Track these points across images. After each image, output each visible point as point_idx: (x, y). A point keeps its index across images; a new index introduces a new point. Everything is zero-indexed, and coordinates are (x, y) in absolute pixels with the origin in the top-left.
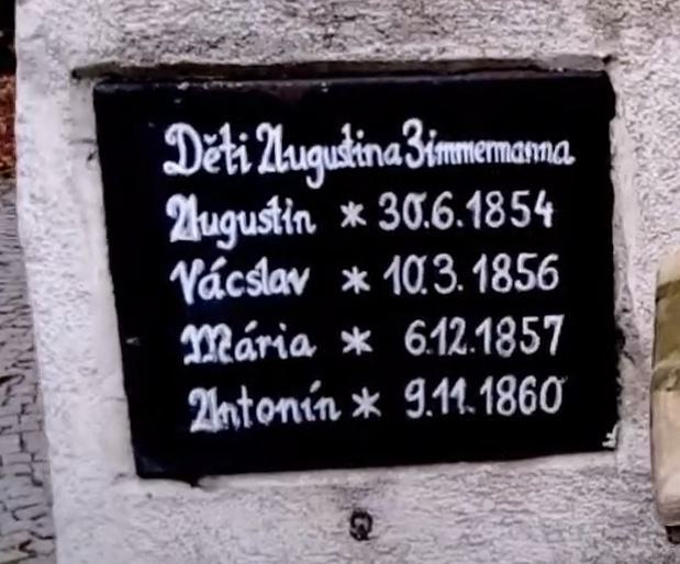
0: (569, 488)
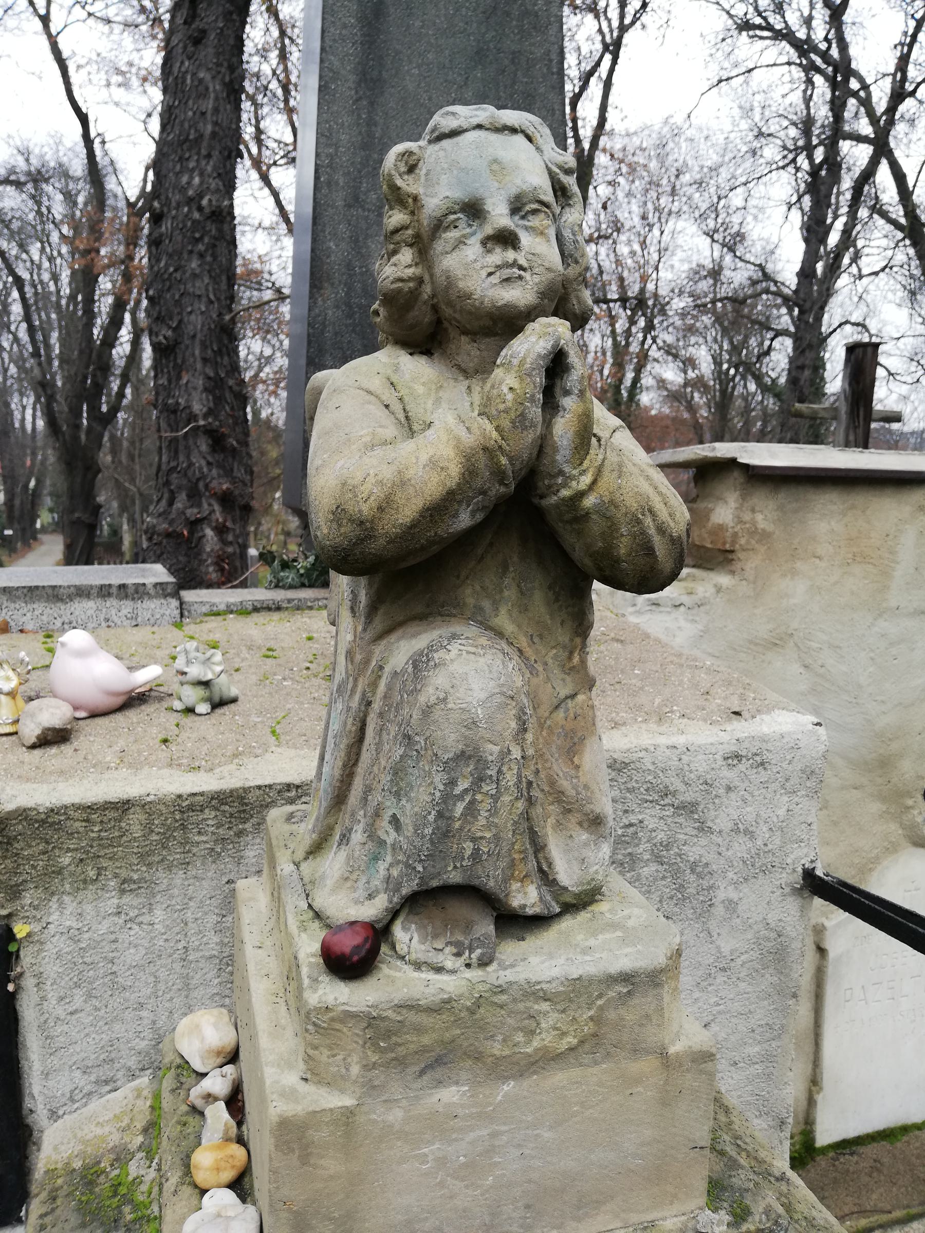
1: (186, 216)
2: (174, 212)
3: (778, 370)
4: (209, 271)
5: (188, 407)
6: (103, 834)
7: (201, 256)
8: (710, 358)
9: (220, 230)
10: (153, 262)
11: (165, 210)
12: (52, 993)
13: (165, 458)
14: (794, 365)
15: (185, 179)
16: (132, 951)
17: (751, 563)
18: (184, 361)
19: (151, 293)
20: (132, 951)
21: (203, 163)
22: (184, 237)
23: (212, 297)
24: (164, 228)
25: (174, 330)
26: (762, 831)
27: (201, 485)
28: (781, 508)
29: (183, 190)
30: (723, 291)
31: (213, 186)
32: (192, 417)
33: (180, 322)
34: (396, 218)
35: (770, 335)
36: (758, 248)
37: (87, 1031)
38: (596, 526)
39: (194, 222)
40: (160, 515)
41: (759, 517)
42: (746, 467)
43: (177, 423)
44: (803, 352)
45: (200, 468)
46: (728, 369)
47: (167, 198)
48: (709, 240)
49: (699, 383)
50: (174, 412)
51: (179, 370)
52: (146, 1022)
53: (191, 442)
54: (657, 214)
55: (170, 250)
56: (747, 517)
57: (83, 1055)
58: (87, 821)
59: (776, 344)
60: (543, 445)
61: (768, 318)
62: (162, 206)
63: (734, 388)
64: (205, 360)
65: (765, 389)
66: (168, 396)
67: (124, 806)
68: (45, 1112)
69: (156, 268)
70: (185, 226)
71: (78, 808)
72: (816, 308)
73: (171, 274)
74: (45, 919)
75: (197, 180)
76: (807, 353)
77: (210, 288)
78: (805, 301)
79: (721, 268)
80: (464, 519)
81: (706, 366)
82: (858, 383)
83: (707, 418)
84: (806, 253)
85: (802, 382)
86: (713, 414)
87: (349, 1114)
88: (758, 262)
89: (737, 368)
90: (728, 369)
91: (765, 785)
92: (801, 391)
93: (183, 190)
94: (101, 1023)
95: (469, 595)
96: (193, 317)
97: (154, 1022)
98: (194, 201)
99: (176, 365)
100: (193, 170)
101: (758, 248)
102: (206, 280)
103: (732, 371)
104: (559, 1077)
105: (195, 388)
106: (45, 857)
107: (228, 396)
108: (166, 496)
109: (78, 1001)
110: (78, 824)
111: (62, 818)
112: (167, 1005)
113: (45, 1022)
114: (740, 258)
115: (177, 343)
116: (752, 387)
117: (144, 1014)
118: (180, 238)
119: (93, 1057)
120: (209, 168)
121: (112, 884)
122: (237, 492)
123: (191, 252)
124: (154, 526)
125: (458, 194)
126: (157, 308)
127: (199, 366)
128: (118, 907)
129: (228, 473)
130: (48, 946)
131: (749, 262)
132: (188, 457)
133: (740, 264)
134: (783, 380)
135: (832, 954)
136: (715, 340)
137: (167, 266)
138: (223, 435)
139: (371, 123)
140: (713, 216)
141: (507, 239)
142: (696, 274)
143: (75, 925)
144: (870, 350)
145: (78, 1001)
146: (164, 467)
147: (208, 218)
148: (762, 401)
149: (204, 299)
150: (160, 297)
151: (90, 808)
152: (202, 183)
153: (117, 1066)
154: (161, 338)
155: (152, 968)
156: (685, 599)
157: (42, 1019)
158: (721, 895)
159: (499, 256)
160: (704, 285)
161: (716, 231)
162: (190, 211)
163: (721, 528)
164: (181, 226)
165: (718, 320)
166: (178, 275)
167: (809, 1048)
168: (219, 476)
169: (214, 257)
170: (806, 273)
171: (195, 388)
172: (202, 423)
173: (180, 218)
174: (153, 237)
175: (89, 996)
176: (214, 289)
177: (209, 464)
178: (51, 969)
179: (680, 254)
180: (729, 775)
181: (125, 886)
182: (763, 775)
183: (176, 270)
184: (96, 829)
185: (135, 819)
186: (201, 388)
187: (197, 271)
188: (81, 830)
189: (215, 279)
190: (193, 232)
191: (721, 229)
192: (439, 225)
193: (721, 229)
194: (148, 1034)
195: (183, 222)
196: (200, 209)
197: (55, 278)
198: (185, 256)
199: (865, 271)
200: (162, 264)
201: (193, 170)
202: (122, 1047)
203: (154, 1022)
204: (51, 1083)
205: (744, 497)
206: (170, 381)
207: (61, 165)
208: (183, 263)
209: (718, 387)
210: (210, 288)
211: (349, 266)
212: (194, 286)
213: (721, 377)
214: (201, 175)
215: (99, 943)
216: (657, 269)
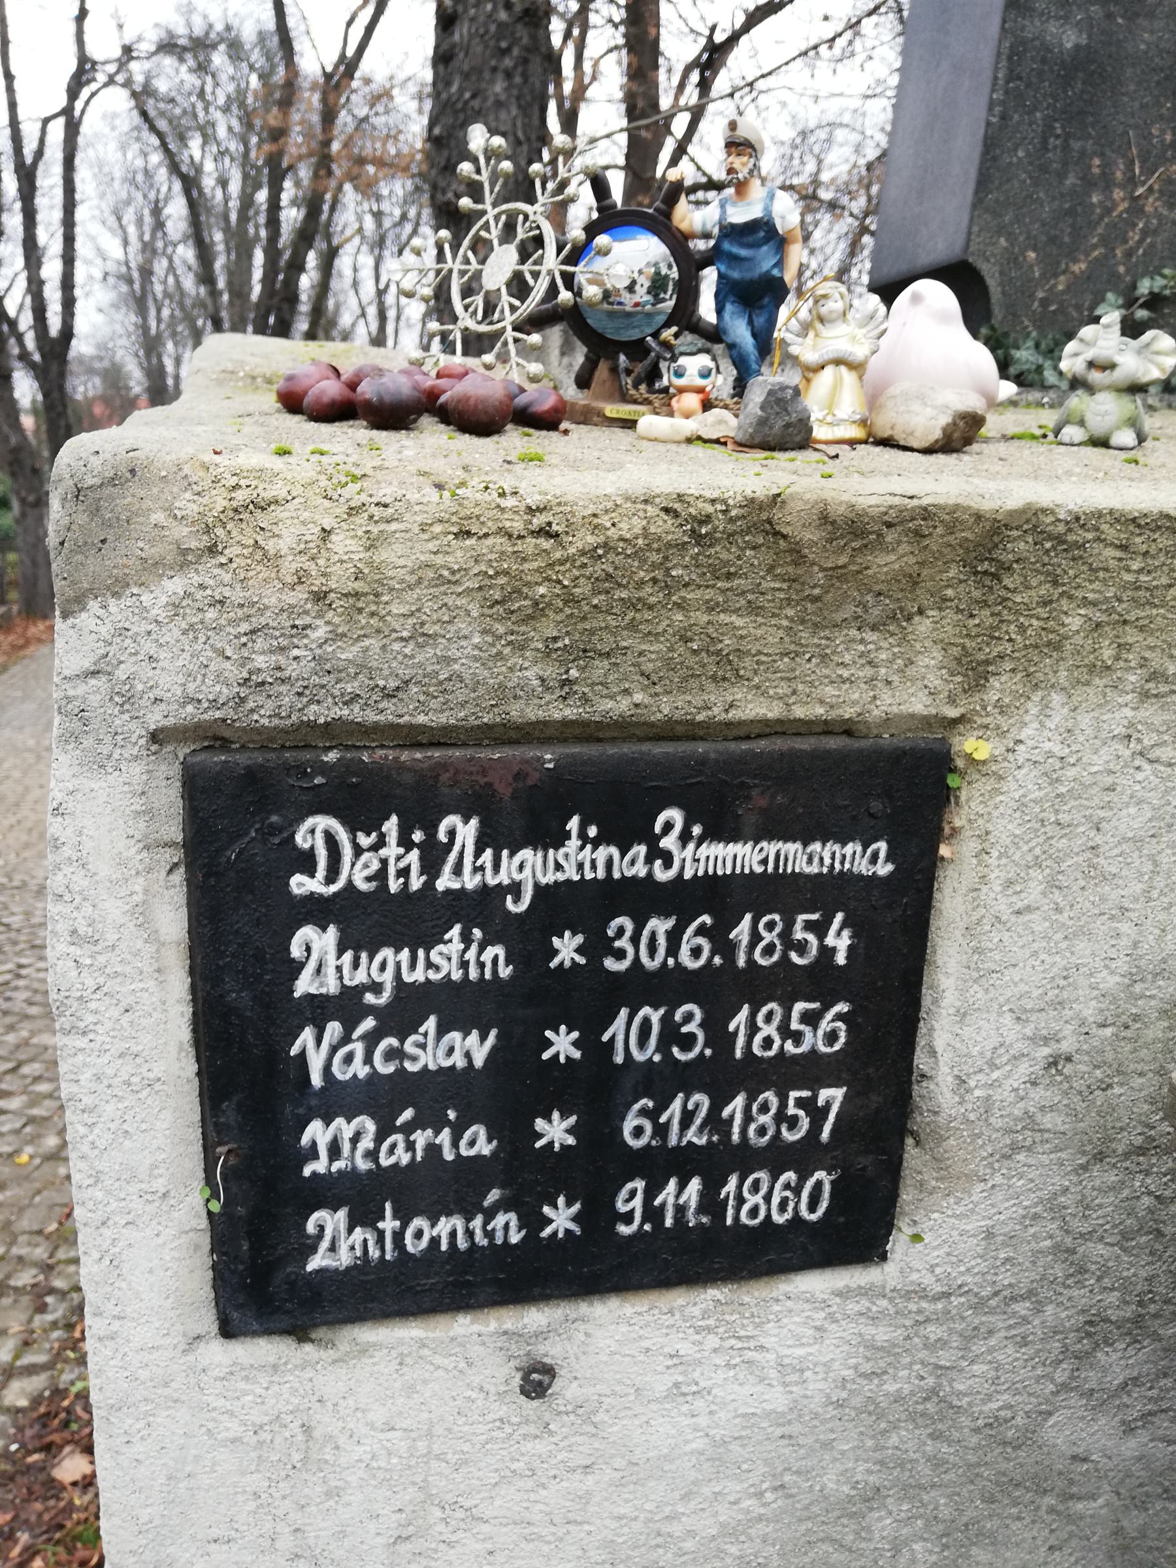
0: (822, 1315)
1: (490, 16)
2: (472, 11)
4: (518, 98)
6: (1144, 578)
7: (508, 75)
10: (440, 86)
11: (460, 8)
12: (997, 872)
16: (1132, 810)
20: (1132, 810)
22: (486, 47)
23: (520, 134)
37: (1036, 946)
39: (501, 25)
52: (1124, 942)
57: (1023, 988)
58: (1124, 548)
68: (950, 1079)
69: (444, 96)
70: (487, 32)
71: (1117, 520)
73: (466, 103)
74: (1014, 734)
77: (519, 123)
94: (1059, 936)
97: (1135, 944)
102: (514, 111)
106: (1042, 612)
109: (1034, 893)
110: (1110, 552)
111: (1090, 536)
112: (1161, 916)
113: (979, 922)
117: (1125, 927)
119: (1036, 993)
121: (1133, 678)
123: (494, 70)
126: (445, 153)
128: (1131, 725)
130: (1010, 785)
137: (461, 90)
143: (1058, 750)
145: (1034, 893)
147: (520, 19)
150: (450, 136)
151: (1135, 522)
153: (1068, 1013)
155: (1150, 848)
157: (975, 916)
162: (495, 9)
164: (482, 31)
166: (476, 104)
169: (525, 76)
173: (482, 19)
174: (441, 50)
175: (1053, 885)
176: (524, 125)
178: (1004, 828)
183: (474, 96)
184: (1135, 566)
187: (503, 97)
188: (1112, 564)
189: (524, 109)
190: (498, 40)
194: (1122, 965)
195: (485, 24)
197: (223, 183)
198: (487, 75)
200: (454, 89)
202: (1083, 982)
203: (1135, 944)
204: (967, 1032)
207: (228, 28)
208: (483, 85)
210: (519, 123)
215: (1086, 787)
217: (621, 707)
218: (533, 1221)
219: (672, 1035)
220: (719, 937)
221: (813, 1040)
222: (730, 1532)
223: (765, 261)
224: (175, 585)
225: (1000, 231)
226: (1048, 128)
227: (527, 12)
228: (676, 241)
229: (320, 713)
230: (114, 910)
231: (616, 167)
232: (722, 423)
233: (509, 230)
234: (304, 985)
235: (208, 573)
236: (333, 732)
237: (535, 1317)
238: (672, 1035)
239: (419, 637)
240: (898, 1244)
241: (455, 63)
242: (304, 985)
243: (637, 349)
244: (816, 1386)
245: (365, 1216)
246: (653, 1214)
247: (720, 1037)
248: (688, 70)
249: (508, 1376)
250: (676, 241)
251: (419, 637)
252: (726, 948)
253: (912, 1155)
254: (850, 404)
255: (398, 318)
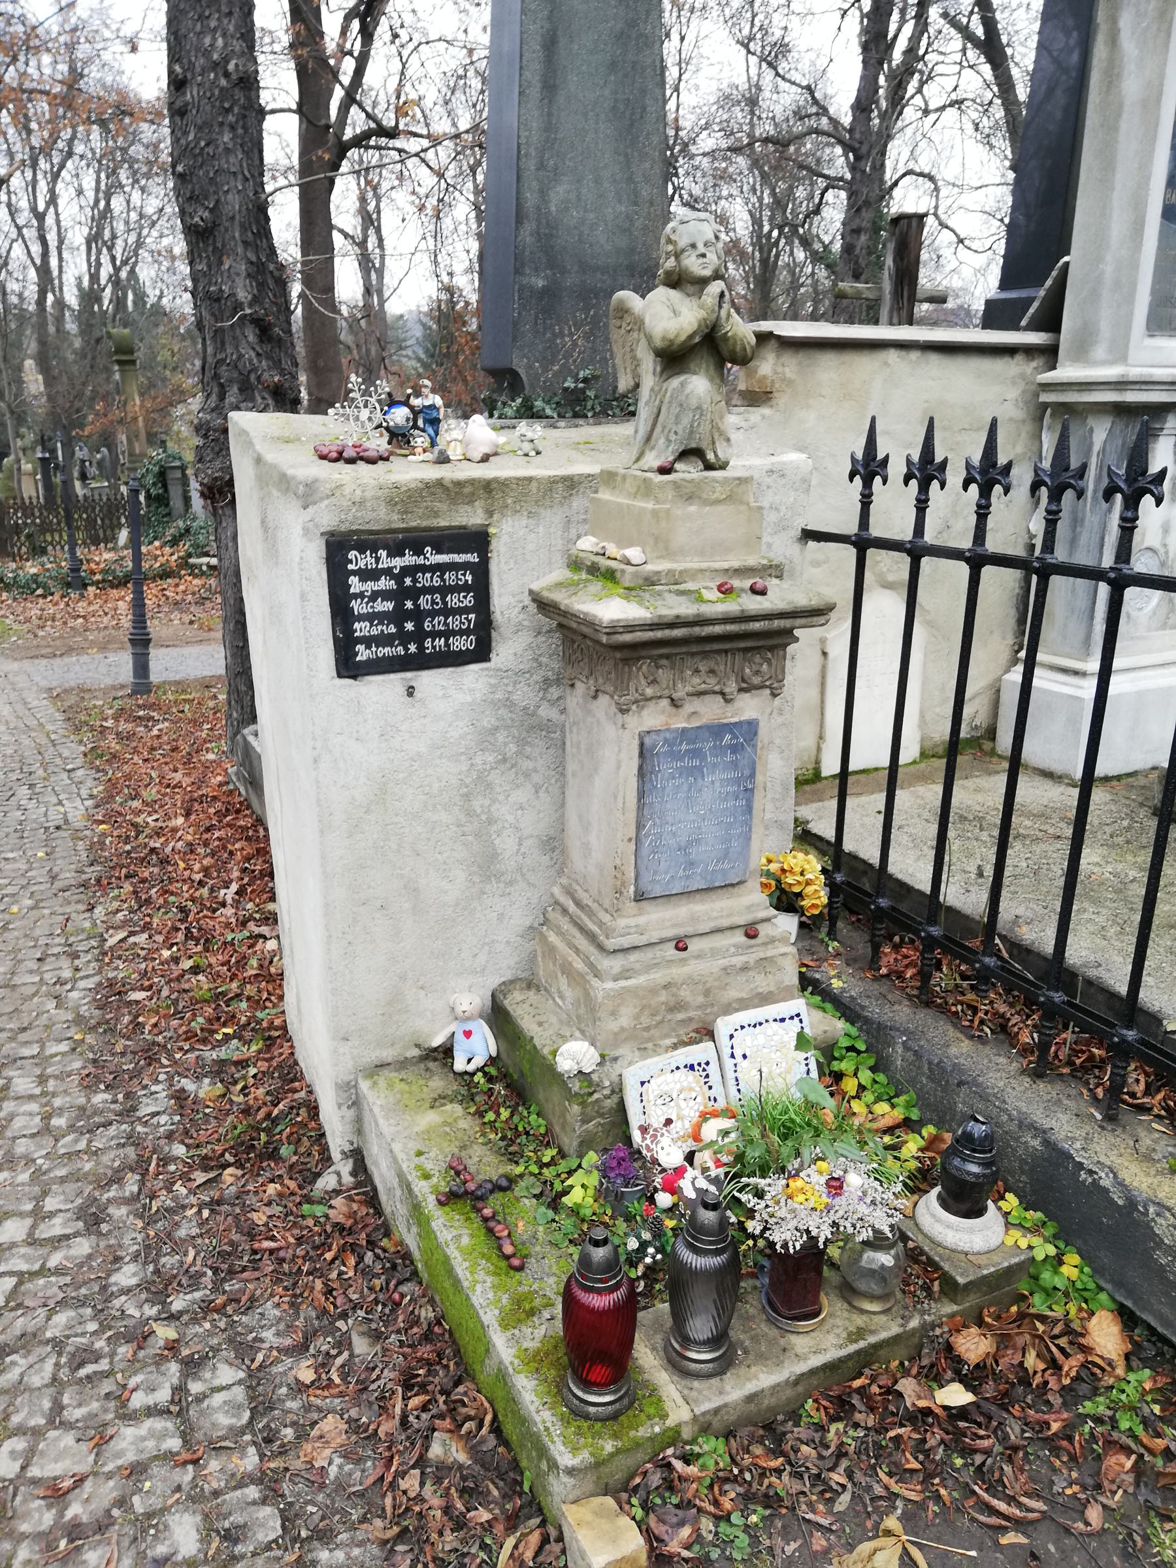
3: (832, 231)
5: (233, 295)
7: (233, 128)
8: (747, 217)
9: (248, 98)
11: (189, 76)
13: (210, 350)
14: (848, 228)
15: (207, 41)
17: (781, 400)
18: (224, 245)
19: (180, 168)
21: (226, 21)
24: (189, 96)
25: (212, 211)
26: (783, 508)
27: (253, 377)
28: (800, 364)
29: (207, 53)
30: (766, 128)
31: (237, 48)
32: (238, 306)
33: (217, 201)
34: (670, 248)
35: (821, 183)
36: (805, 65)
38: (731, 342)
39: (222, 89)
40: (213, 410)
41: (787, 370)
42: (779, 337)
43: (221, 312)
44: (858, 210)
45: (250, 360)
46: (771, 231)
47: (190, 62)
48: (743, 51)
49: (734, 249)
50: (218, 300)
51: (219, 254)
53: (238, 332)
54: (675, 14)
55: (199, 122)
56: (780, 369)
59: (830, 196)
60: (718, 318)
61: (818, 161)
62: (185, 71)
63: (777, 256)
64: (246, 243)
65: (817, 258)
66: (210, 284)
67: (530, 479)
70: (213, 95)
72: (874, 152)
75: (220, 42)
76: (864, 213)
78: (861, 143)
79: (759, 88)
80: (697, 339)
81: (742, 226)
82: (902, 259)
83: (744, 297)
84: (863, 78)
85: (857, 251)
86: (753, 291)
87: (668, 510)
88: (804, 83)
89: (781, 228)
90: (771, 231)
91: (784, 486)
92: (856, 262)
93: (207, 53)
95: (692, 366)
96: (230, 196)
98: (219, 66)
99: (215, 249)
100: (215, 30)
101: (805, 65)
103: (775, 233)
104: (720, 508)
105: (238, 275)
107: (271, 282)
108: (216, 390)
114: (783, 78)
115: (215, 225)
116: (800, 255)
118: (208, 108)
120: (231, 28)
122: (287, 385)
123: (221, 124)
124: (208, 422)
125: (689, 242)
127: (240, 250)
129: (277, 364)
131: (794, 83)
132: (237, 348)
133: (784, 85)
134: (837, 247)
135: (831, 656)
136: (754, 190)
137: (197, 140)
138: (270, 324)
139: (550, 114)
140: (749, 15)
141: (704, 255)
142: (726, 100)
144: (914, 222)
145: (512, 565)
146: (210, 359)
148: (813, 274)
149: (240, 177)
150: (191, 174)
151: (518, 479)
152: (226, 45)
154: (197, 219)
156: (743, 424)
158: (764, 540)
159: (702, 260)
160: (739, 115)
161: (751, 38)
163: (764, 377)
165: (755, 164)
166: (210, 150)
167: (818, 716)
168: (269, 368)
170: (862, 106)
171: (238, 275)
172: (248, 311)
177: (258, 355)
178: (503, 549)
179: (706, 71)
180: (768, 480)
181: (530, 515)
182: (783, 481)
183: (207, 145)
185: (534, 485)
186: (244, 274)
187: (230, 146)
191: (759, 36)
192: (683, 251)
193: (759, 36)
196: (227, 75)
199: (932, 107)
200: (191, 137)
201: (215, 30)
205: (778, 357)
206: (209, 267)
209: (757, 254)
211: (538, 209)
212: (228, 162)
213: (763, 243)
214: (224, 35)
216: (677, 89)
217: (414, 524)
218: (406, 649)
219: (434, 602)
220: (441, 577)
221: (466, 603)
222: (462, 737)
223: (435, 414)
224: (326, 502)
225: (524, 356)
226: (537, 317)
227: (241, 79)
228: (412, 408)
229: (354, 528)
230: (314, 572)
231: (290, 110)
232: (429, 456)
233: (366, 406)
234: (352, 591)
235: (332, 499)
236: (356, 532)
237: (409, 675)
238: (434, 602)
239: (373, 510)
240: (493, 656)
241: (189, 117)
242: (352, 591)
243: (404, 435)
244: (478, 695)
245: (368, 647)
246: (434, 647)
247: (445, 603)
248: (348, 18)
249: (402, 691)
250: (412, 408)
251: (373, 510)
252: (443, 580)
253: (494, 634)
254: (459, 451)
255: (61, 241)
